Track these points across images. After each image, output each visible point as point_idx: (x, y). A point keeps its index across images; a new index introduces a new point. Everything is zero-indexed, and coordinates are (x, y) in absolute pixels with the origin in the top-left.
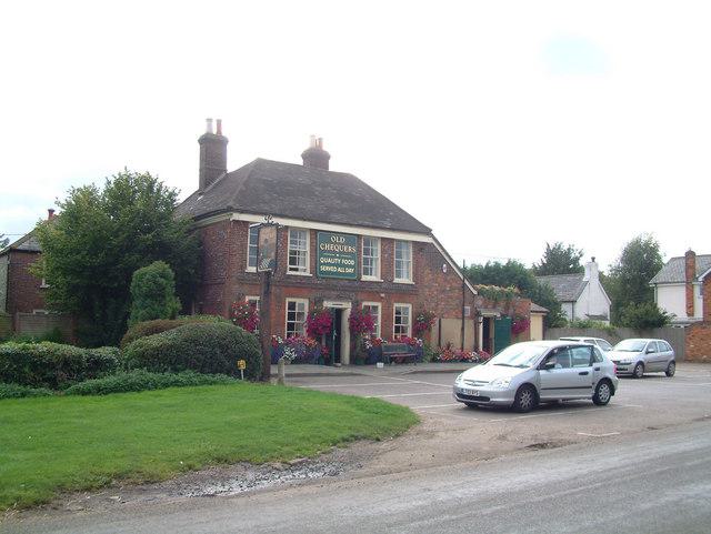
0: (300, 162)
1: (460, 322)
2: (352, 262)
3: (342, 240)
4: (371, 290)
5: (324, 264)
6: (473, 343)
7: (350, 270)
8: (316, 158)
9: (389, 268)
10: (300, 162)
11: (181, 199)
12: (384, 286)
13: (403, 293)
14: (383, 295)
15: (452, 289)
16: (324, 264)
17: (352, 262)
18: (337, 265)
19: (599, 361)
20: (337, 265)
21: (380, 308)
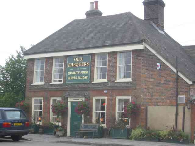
0: (85, 17)
1: (175, 108)
2: (87, 72)
3: (81, 59)
4: (98, 89)
5: (71, 76)
6: (174, 124)
7: (85, 77)
8: (94, 14)
9: (47, 76)
10: (85, 17)
11: (103, 15)
12: (108, 85)
13: (122, 89)
14: (105, 91)
15: (167, 82)
16: (71, 76)
17: (87, 72)
18: (77, 75)
19: (118, 112)
20: (77, 75)
21: (55, 98)
